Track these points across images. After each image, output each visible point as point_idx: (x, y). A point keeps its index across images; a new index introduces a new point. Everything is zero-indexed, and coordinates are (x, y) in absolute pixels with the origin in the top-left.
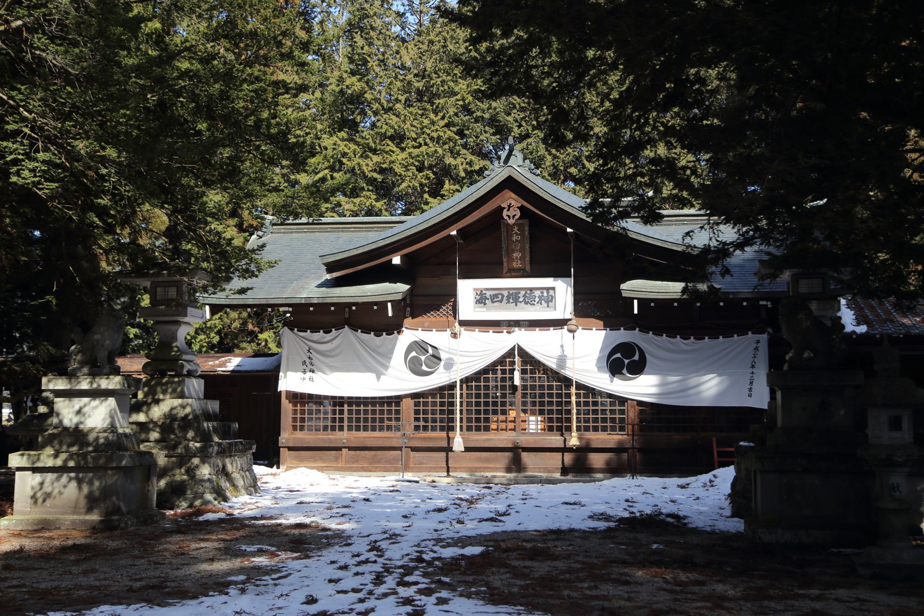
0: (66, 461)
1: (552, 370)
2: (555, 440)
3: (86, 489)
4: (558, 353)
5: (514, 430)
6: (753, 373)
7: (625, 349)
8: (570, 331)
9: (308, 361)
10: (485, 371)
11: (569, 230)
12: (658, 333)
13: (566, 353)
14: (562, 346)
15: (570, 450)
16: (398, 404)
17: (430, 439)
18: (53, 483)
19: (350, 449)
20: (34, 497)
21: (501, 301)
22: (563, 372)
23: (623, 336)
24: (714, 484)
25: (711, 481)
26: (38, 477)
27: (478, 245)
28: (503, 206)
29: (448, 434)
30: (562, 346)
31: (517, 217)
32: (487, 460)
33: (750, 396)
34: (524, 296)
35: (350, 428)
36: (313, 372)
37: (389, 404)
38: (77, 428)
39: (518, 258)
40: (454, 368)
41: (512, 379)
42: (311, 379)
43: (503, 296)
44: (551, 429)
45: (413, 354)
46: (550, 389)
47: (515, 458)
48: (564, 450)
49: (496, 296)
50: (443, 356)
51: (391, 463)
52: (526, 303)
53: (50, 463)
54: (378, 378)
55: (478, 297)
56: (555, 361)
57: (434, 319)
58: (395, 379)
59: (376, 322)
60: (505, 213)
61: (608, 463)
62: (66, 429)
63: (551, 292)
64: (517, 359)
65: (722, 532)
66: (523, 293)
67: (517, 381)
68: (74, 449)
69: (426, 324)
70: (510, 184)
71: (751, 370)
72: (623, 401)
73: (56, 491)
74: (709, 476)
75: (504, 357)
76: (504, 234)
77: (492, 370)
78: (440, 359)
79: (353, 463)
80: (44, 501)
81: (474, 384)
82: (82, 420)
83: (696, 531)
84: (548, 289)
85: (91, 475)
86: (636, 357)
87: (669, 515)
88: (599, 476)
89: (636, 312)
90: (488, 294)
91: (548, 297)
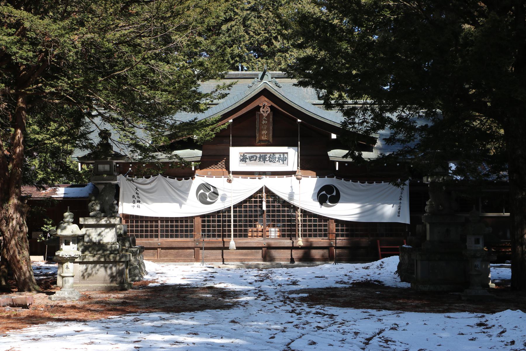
0: (99, 258)
1: (284, 201)
2: (287, 242)
3: (109, 272)
4: (289, 191)
5: (262, 236)
6: (400, 203)
7: (328, 189)
8: (298, 179)
9: (136, 195)
10: (245, 201)
11: (299, 120)
12: (347, 179)
13: (294, 191)
14: (291, 187)
15: (297, 248)
16: (192, 221)
17: (212, 242)
18: (92, 269)
19: (162, 248)
20: (83, 276)
21: (255, 160)
22: (292, 202)
23: (327, 181)
24: (383, 266)
25: (381, 265)
26: (84, 267)
27: (244, 127)
28: (260, 105)
29: (223, 239)
30: (291, 187)
31: (268, 112)
32: (246, 254)
33: (399, 216)
34: (269, 157)
35: (162, 236)
36: (139, 202)
37: (186, 221)
38: (99, 242)
39: (265, 135)
40: (227, 200)
41: (261, 207)
42: (138, 207)
43: (257, 157)
44: (283, 236)
45: (202, 191)
46: (281, 212)
47: (268, 253)
48: (292, 248)
49: (252, 157)
50: (220, 192)
51: (187, 257)
52: (270, 161)
53: (91, 259)
54: (181, 206)
55: (242, 158)
56: (287, 196)
57: (213, 170)
58: (191, 207)
59: (183, 172)
60: (261, 109)
61: (323, 256)
62: (94, 243)
63: (286, 155)
64: (264, 195)
65: (401, 288)
66: (269, 155)
67: (264, 208)
68: (100, 252)
69: (209, 173)
70: (265, 92)
71: (399, 201)
72: (326, 219)
73: (94, 272)
74: (379, 262)
75: (257, 193)
76: (257, 120)
77: (249, 201)
78: (217, 194)
79: (164, 257)
80: (88, 277)
81: (238, 209)
82: (101, 238)
83: (388, 287)
84: (284, 153)
85: (111, 265)
86: (334, 194)
87: (375, 281)
88: (318, 263)
89: (337, 169)
90: (248, 156)
91: (284, 158)
